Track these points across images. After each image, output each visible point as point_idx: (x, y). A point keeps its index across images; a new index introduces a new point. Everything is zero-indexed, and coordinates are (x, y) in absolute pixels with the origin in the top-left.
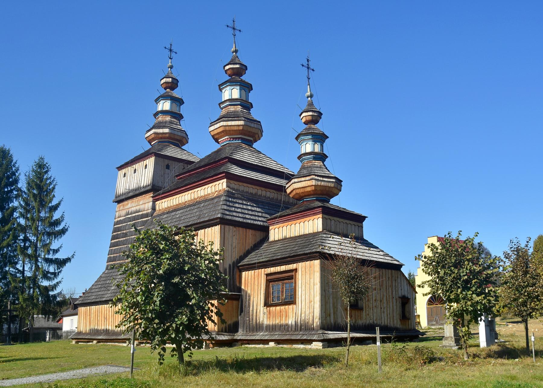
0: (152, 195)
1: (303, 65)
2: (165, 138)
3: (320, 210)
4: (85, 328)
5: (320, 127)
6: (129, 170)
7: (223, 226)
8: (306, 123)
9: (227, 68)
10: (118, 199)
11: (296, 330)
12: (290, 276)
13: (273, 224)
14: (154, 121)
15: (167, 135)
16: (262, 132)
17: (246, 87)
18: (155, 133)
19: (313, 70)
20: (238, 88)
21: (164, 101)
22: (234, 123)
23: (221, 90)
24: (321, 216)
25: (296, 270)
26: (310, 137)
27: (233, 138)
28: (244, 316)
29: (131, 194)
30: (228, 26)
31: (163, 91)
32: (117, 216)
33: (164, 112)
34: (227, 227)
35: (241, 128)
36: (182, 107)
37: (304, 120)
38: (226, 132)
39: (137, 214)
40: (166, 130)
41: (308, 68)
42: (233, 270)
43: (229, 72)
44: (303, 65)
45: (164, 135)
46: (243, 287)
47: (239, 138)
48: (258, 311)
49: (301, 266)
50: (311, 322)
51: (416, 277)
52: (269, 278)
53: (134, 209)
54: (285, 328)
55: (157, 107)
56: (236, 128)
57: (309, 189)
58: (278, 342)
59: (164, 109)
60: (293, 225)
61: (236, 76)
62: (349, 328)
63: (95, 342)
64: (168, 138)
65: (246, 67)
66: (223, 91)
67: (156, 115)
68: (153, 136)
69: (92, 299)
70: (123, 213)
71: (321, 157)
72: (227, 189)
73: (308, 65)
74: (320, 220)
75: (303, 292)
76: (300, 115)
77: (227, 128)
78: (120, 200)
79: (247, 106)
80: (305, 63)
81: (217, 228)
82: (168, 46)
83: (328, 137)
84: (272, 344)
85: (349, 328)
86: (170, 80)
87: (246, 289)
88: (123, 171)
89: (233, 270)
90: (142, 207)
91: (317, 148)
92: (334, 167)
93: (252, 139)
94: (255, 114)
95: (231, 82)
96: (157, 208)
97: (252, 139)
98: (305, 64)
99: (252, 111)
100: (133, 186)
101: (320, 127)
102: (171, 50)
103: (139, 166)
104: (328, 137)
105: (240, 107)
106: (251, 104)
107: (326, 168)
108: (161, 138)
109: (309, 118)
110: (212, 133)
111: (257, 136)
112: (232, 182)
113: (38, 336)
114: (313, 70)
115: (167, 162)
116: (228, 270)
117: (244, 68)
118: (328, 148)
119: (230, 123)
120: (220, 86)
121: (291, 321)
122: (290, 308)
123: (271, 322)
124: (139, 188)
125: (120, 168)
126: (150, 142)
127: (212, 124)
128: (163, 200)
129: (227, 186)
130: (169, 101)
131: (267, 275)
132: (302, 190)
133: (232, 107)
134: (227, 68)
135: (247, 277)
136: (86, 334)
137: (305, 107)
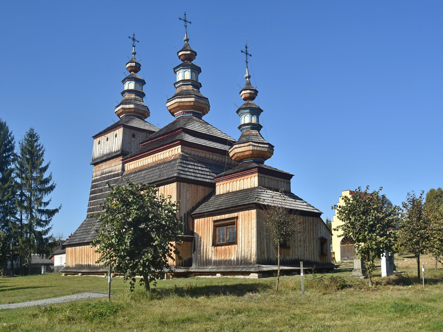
0: (121, 159)
2: (131, 112)
3: (256, 170)
4: (72, 264)
5: (256, 102)
7: (179, 183)
8: (245, 99)
9: (180, 54)
10: (95, 162)
11: (237, 264)
12: (233, 222)
14: (121, 99)
15: (133, 110)
16: (209, 106)
18: (123, 108)
20: (190, 70)
21: (129, 82)
22: (186, 100)
23: (175, 72)
25: (237, 218)
26: (248, 111)
27: (186, 112)
28: (197, 253)
29: (105, 158)
30: (180, 19)
31: (128, 74)
32: (94, 176)
33: (129, 91)
35: (192, 104)
36: (144, 86)
37: (243, 97)
38: (180, 107)
39: (110, 174)
40: (132, 106)
41: (246, 54)
42: (188, 217)
43: (182, 57)
45: (130, 110)
46: (195, 231)
47: (190, 112)
48: (208, 250)
49: (241, 214)
50: (249, 258)
53: (107, 170)
54: (228, 263)
55: (123, 87)
56: (188, 104)
57: (247, 153)
58: (223, 273)
60: (235, 182)
61: (188, 61)
63: (80, 274)
64: (133, 112)
66: (177, 73)
67: (123, 93)
68: (121, 111)
69: (77, 241)
70: (99, 173)
71: (257, 127)
73: (246, 51)
74: (256, 178)
75: (243, 235)
77: (181, 104)
78: (96, 163)
79: (197, 85)
82: (132, 36)
83: (262, 111)
84: (218, 275)
86: (134, 64)
87: (198, 233)
88: (98, 139)
89: (188, 217)
90: (114, 168)
91: (254, 120)
92: (268, 135)
94: (203, 92)
95: (184, 66)
96: (126, 169)
98: (244, 51)
99: (201, 89)
100: (106, 151)
101: (256, 102)
102: (134, 39)
103: (110, 135)
104: (262, 111)
105: (191, 86)
106: (200, 84)
107: (261, 136)
108: (128, 112)
109: (248, 95)
110: (169, 108)
111: (205, 110)
112: (185, 147)
113: (35, 270)
115: (133, 131)
116: (183, 218)
118: (263, 119)
119: (183, 100)
120: (174, 69)
121: (233, 257)
123: (218, 258)
124: (111, 153)
125: (95, 137)
126: (119, 115)
127: (169, 101)
128: (131, 163)
129: (182, 151)
131: (214, 222)
132: (242, 154)
133: (185, 86)
134: (180, 54)
136: (73, 268)
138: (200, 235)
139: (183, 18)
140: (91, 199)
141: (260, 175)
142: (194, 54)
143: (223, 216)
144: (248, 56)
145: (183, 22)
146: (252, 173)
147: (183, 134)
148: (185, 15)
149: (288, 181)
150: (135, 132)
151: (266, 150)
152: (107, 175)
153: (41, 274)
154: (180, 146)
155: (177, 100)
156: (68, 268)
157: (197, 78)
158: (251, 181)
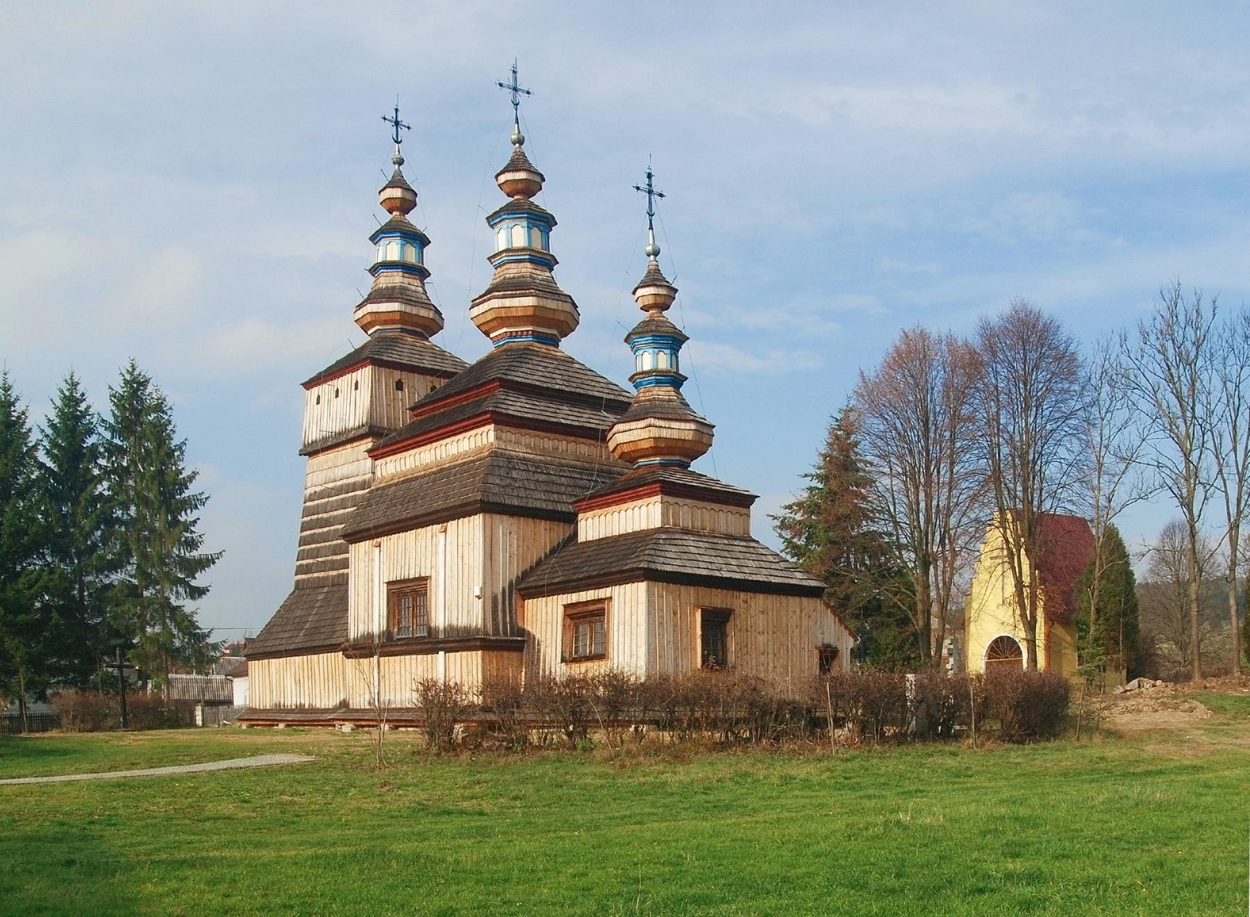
0: (370, 445)
1: (638, 188)
3: (657, 486)
4: (264, 701)
6: (325, 389)
7: (487, 516)
8: (645, 308)
9: (502, 179)
13: (585, 510)
14: (368, 284)
17: (543, 222)
19: (661, 195)
20: (525, 223)
22: (516, 302)
24: (658, 498)
30: (501, 85)
31: (385, 217)
32: (309, 484)
34: (497, 517)
37: (640, 304)
41: (650, 192)
42: (510, 597)
44: (638, 188)
51: (1116, 521)
52: (570, 611)
59: (389, 259)
60: (616, 514)
62: (1233, 612)
63: (281, 726)
65: (541, 176)
67: (374, 270)
69: (270, 645)
72: (496, 444)
73: (650, 185)
74: (659, 506)
75: (621, 639)
76: (634, 293)
78: (312, 451)
79: (546, 261)
80: (643, 184)
81: (478, 520)
82: (391, 115)
85: (1233, 612)
88: (315, 391)
89: (510, 597)
91: (664, 362)
93: (554, 332)
96: (378, 474)
97: (554, 332)
98: (643, 186)
100: (336, 427)
102: (397, 123)
103: (344, 382)
105: (528, 265)
109: (650, 301)
112: (505, 428)
113: (178, 716)
114: (661, 195)
115: (397, 375)
116: (500, 597)
117: (532, 186)
118: (431, 257)
119: (507, 302)
122: (602, 663)
124: (347, 431)
125: (309, 385)
126: (365, 328)
128: (388, 459)
129: (498, 438)
130: (399, 241)
133: (513, 265)
134: (502, 179)
135: (680, 542)
136: (265, 711)
137: (642, 275)
138: (538, 636)
139: (511, 83)
140: (303, 541)
141: (667, 498)
142: (538, 179)
143: (583, 594)
144: (655, 198)
145: (508, 94)
146: (649, 495)
147: (500, 394)
148: (514, 72)
149: (744, 511)
150: (404, 376)
151: (689, 436)
152: (339, 483)
153: (192, 724)
154: (492, 426)
155: (495, 303)
156: (252, 710)
157: (546, 245)
158: (643, 515)
